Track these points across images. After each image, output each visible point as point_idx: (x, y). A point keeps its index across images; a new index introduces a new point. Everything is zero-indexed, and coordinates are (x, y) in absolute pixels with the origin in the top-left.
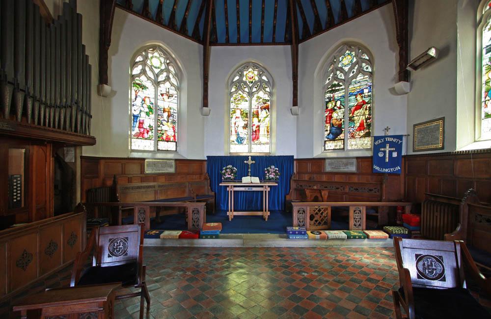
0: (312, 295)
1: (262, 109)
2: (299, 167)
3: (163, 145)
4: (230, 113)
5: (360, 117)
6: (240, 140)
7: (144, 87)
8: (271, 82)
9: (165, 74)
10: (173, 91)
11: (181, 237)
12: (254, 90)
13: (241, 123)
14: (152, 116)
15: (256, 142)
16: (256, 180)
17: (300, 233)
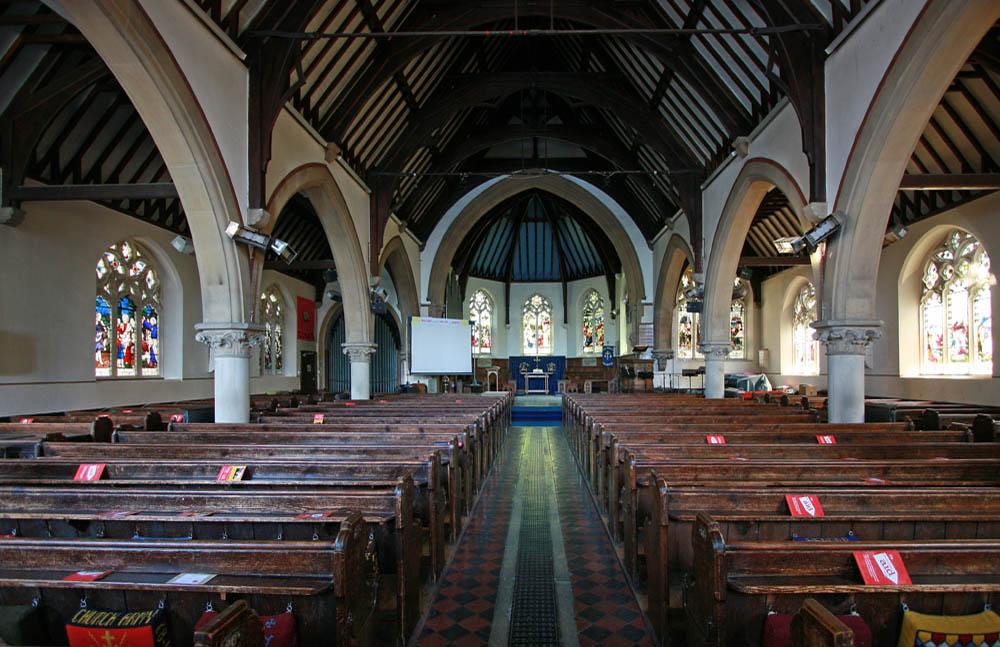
0: (325, 166)
3: (484, 350)
4: (522, 326)
6: (531, 345)
7: (473, 315)
10: (488, 315)
11: (485, 151)
16: (541, 371)
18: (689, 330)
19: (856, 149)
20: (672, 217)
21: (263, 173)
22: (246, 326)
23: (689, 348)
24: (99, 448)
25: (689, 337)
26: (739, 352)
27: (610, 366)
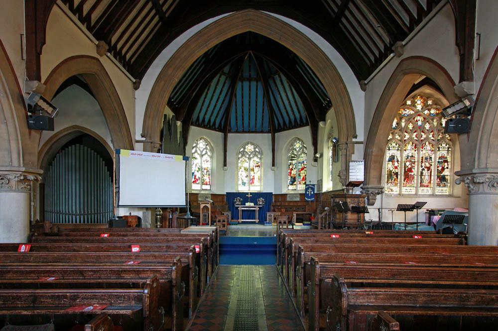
1: (256, 167)
2: (275, 198)
3: (205, 187)
4: (238, 169)
5: (303, 174)
6: (244, 184)
7: (196, 158)
8: (261, 152)
9: (205, 150)
10: (209, 159)
12: (251, 156)
13: (244, 174)
14: (200, 172)
15: (252, 185)
16: (252, 204)
17: (269, 223)
18: (396, 168)
20: (365, 80)
21: (39, 54)
22: (23, 169)
23: (396, 185)
25: (397, 174)
26: (445, 188)
27: (312, 201)
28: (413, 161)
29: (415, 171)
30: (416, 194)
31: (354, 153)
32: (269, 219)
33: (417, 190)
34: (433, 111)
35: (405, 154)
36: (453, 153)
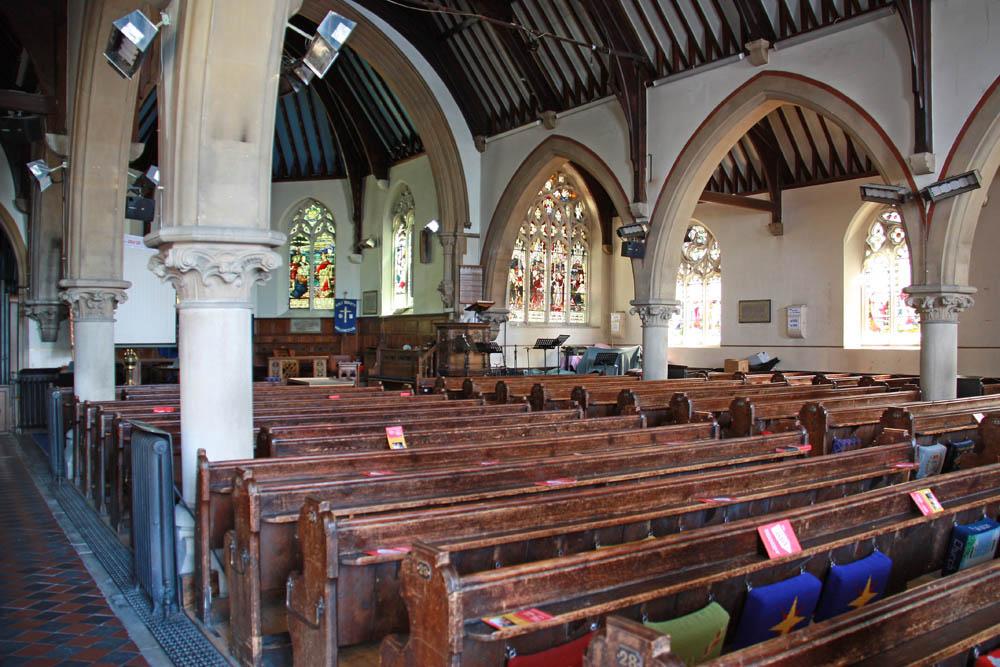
18: (520, 279)
19: (985, 107)
24: (470, 516)
25: (521, 289)
28: (541, 269)
29: (544, 285)
30: (546, 323)
31: (465, 253)
32: (273, 372)
33: (547, 316)
34: (565, 194)
35: (532, 256)
36: (590, 260)
